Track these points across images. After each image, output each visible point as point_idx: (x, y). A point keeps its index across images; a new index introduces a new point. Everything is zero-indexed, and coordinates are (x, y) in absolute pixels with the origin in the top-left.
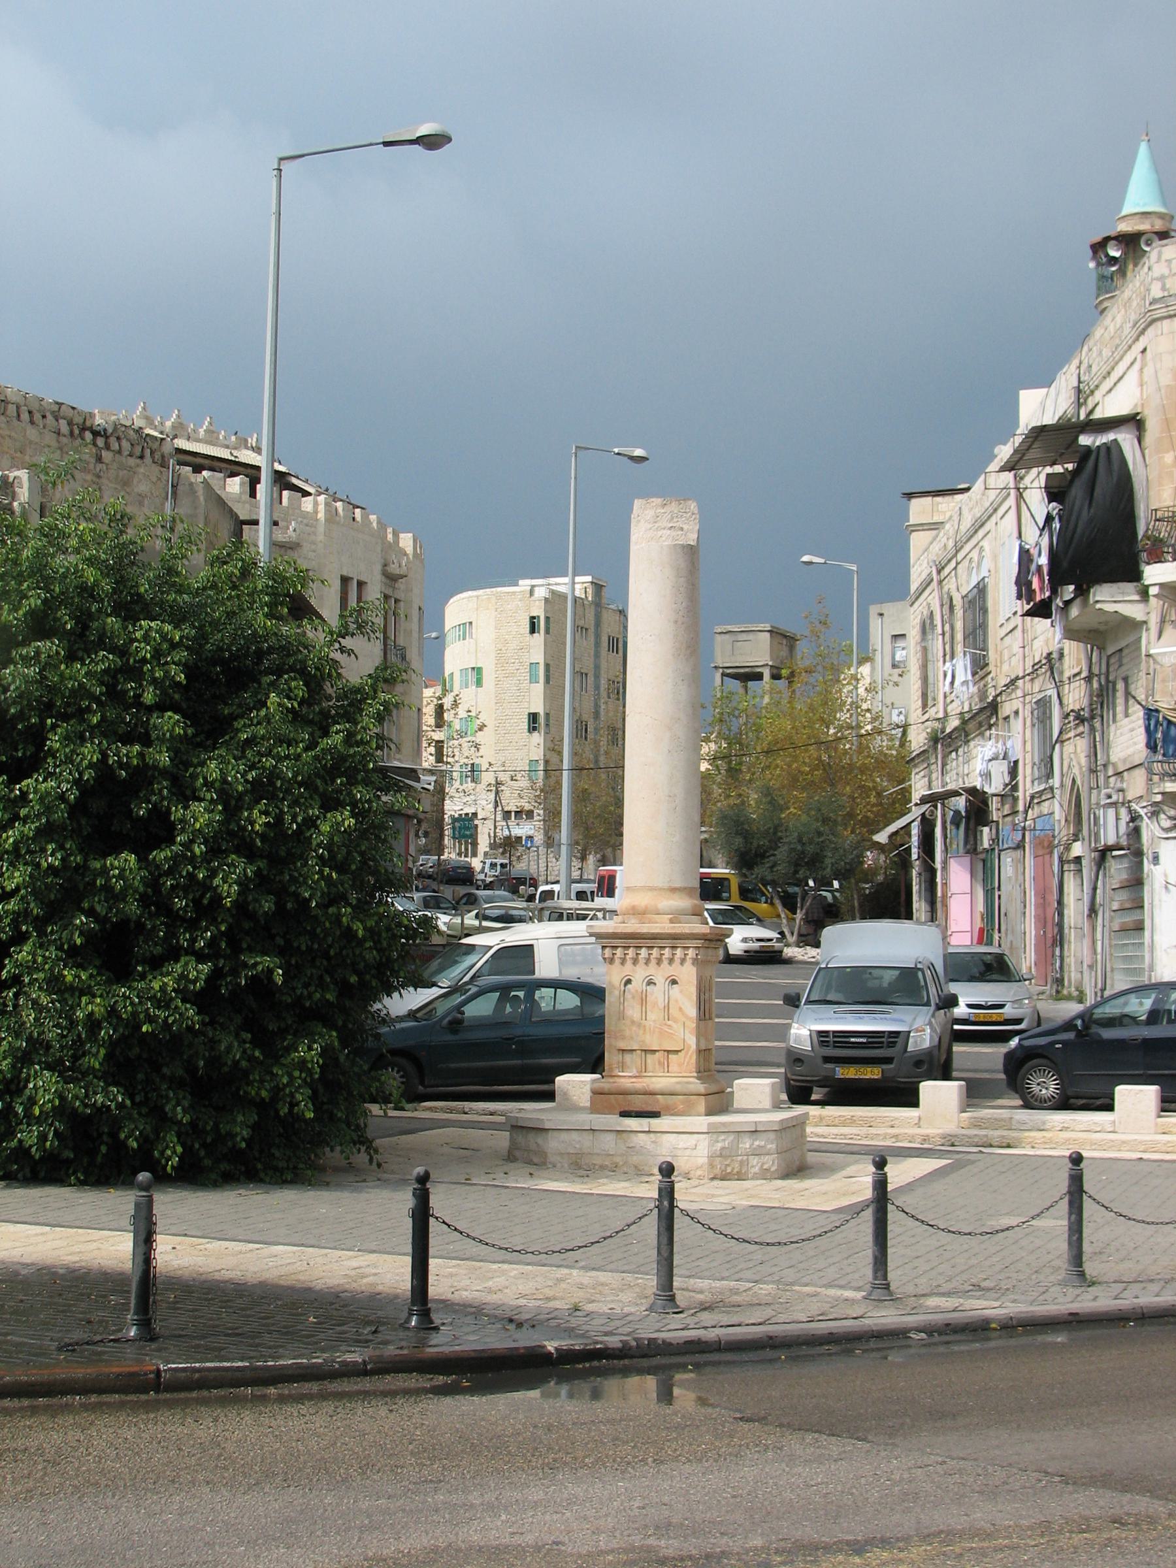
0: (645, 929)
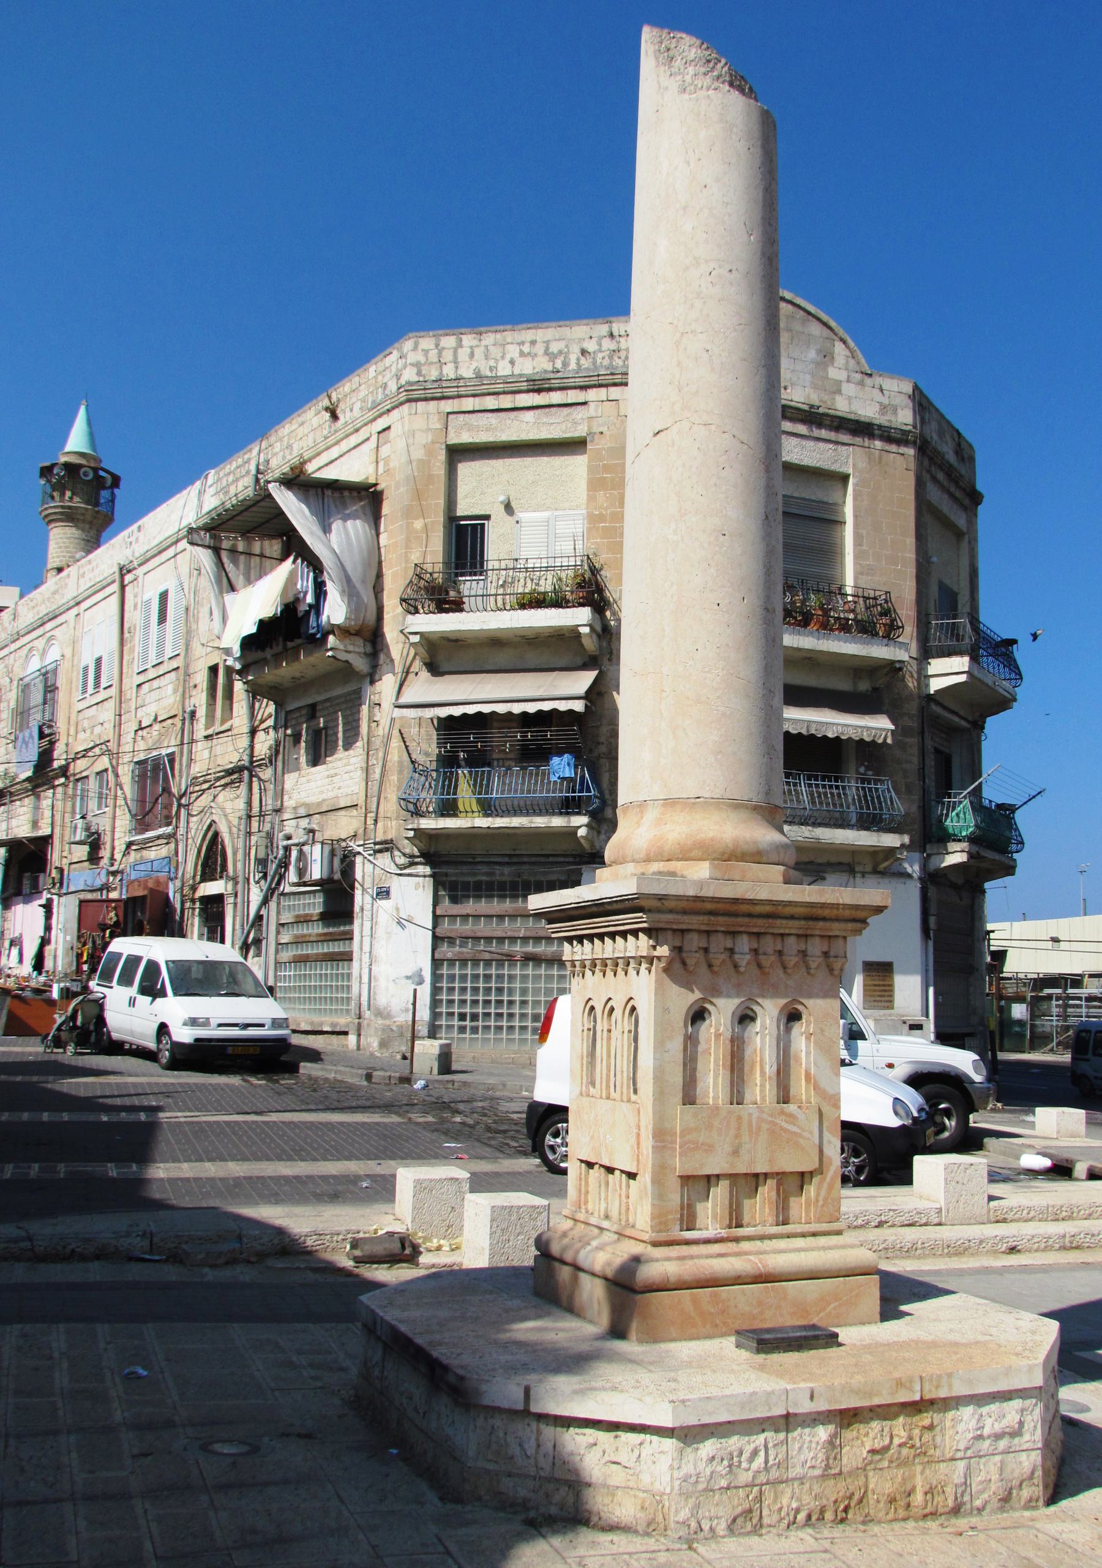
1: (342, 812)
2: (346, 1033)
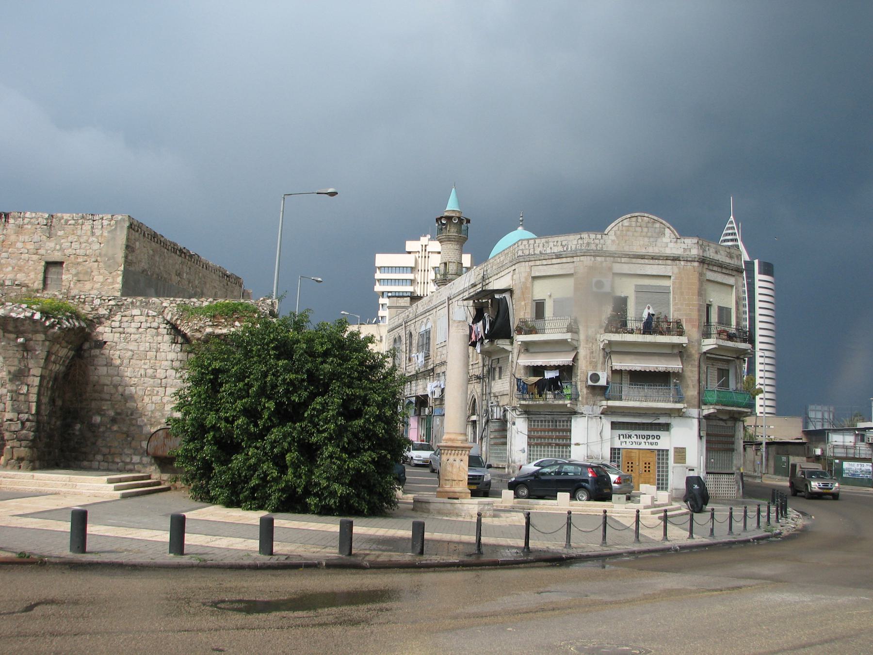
0: (455, 445)
1: (505, 396)
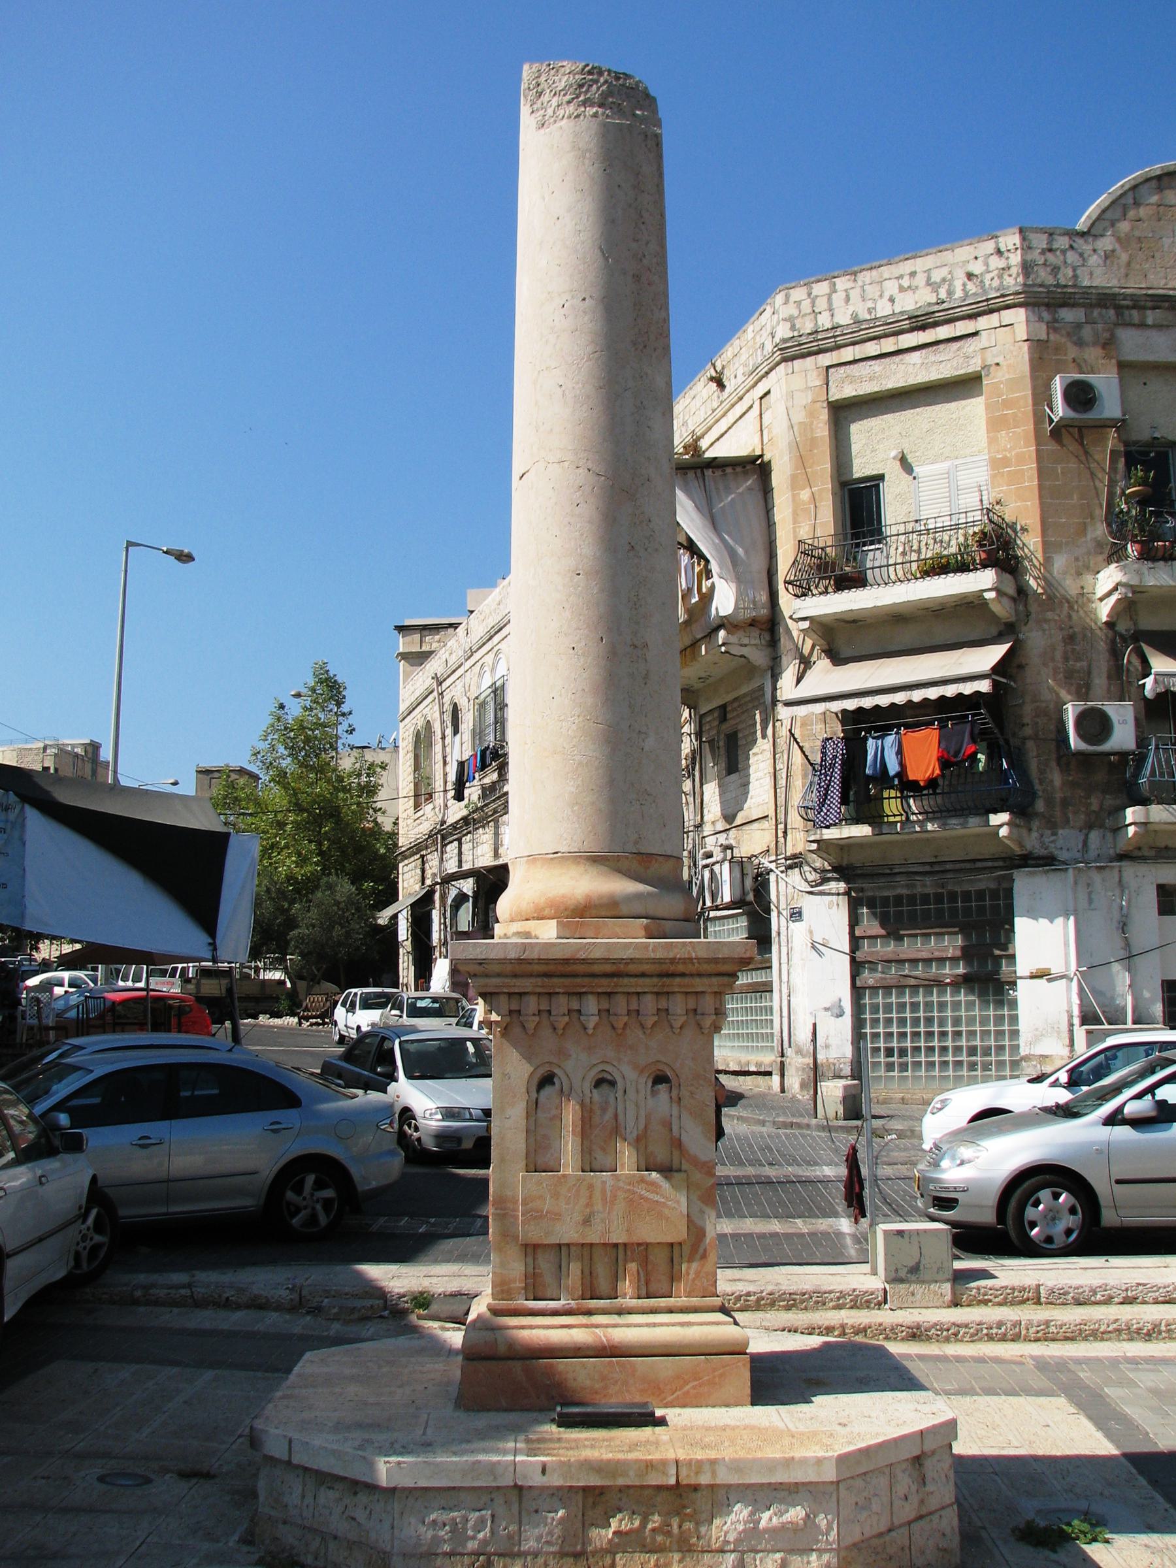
1: (755, 825)
2: (769, 1074)
